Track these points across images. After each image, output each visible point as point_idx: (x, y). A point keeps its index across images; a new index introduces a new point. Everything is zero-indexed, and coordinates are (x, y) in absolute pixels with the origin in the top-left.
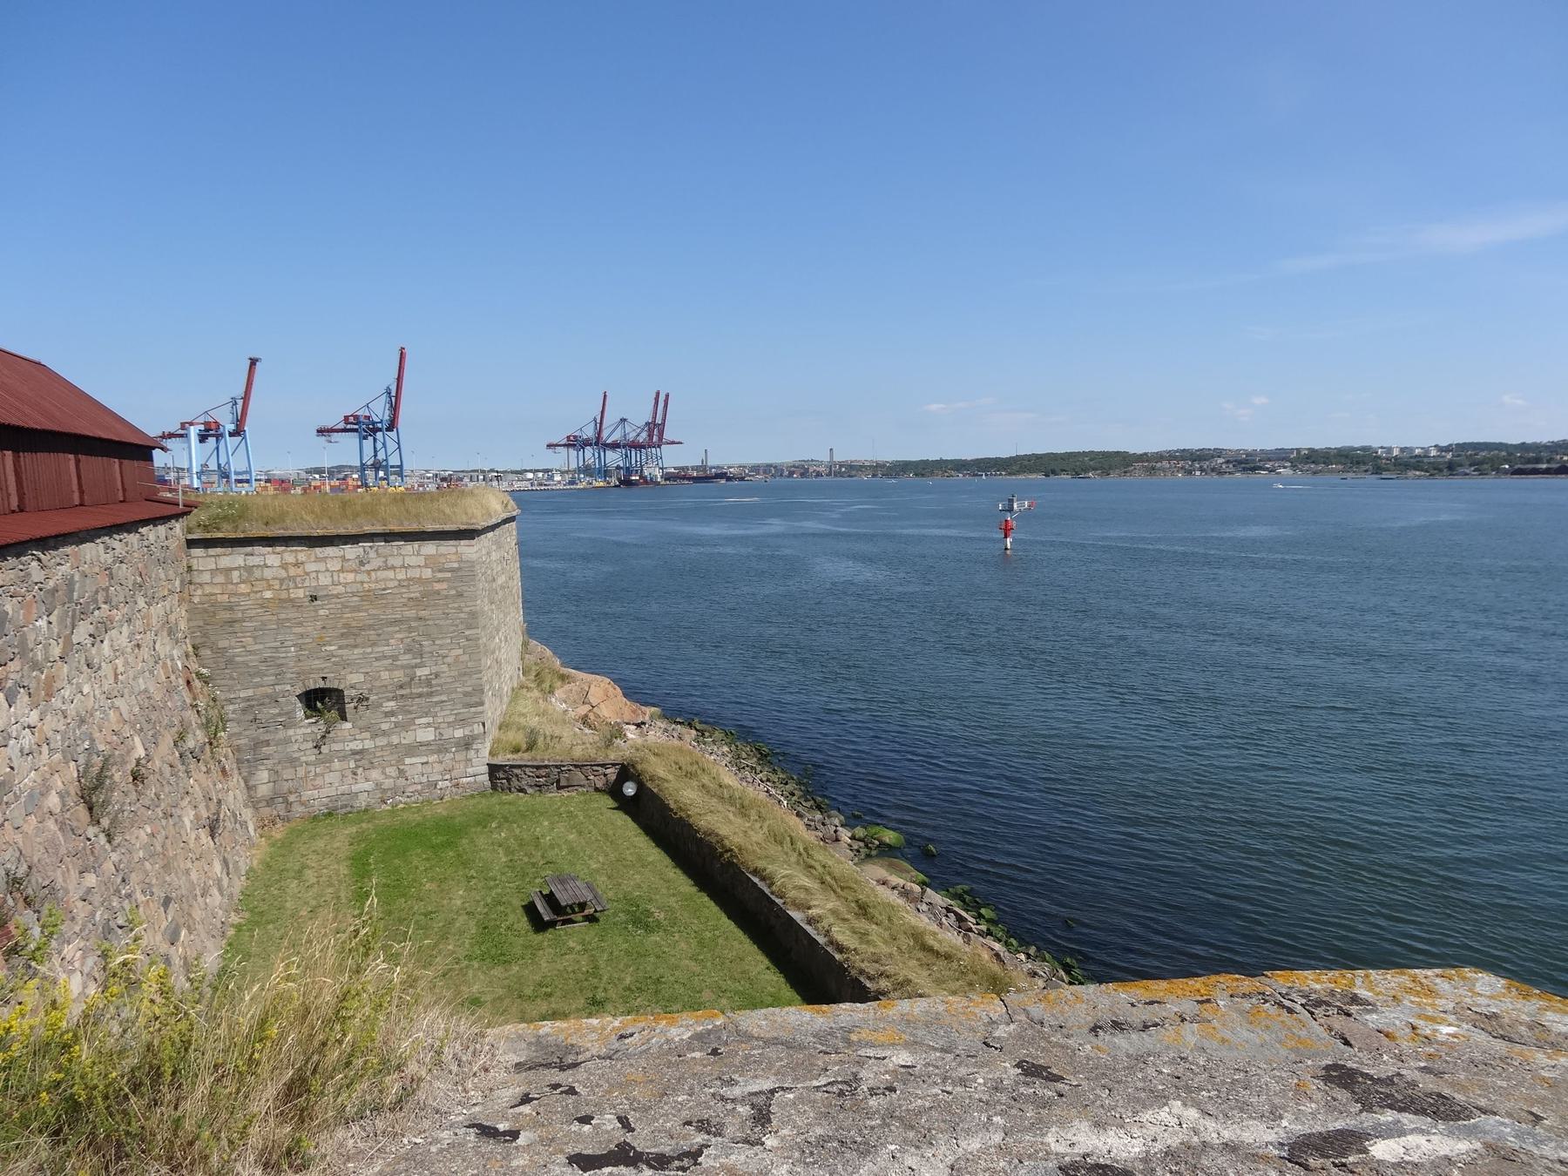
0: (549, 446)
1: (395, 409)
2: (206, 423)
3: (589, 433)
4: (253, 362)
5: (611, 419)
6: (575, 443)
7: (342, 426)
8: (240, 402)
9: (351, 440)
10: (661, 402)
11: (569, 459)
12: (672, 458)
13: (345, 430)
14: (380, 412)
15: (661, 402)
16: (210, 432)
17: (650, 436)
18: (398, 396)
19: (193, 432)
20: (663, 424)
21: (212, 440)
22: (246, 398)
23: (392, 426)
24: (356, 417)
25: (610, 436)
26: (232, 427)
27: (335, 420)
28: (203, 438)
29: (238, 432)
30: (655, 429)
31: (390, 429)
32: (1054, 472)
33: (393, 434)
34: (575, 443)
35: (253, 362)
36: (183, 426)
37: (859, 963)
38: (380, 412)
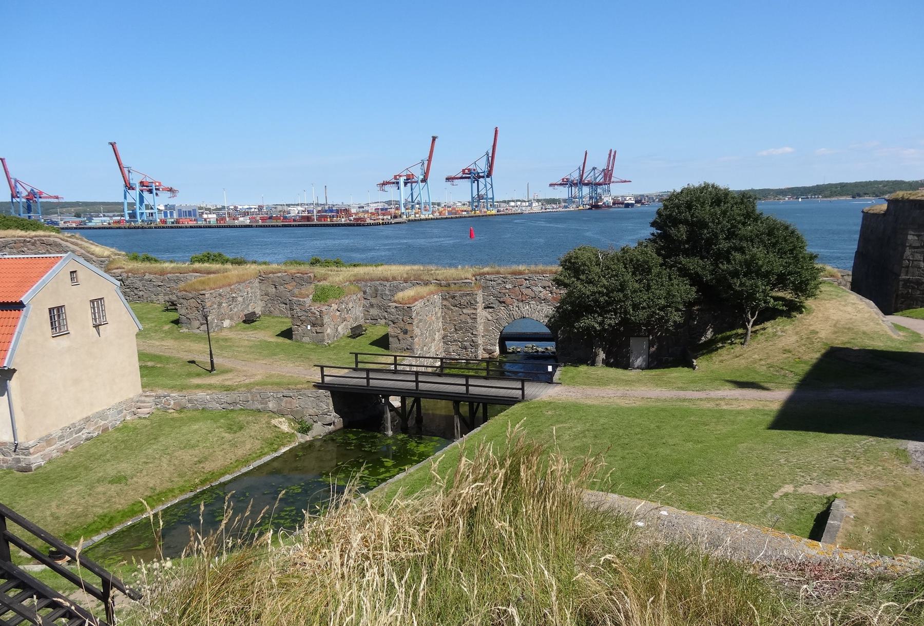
0: (551, 185)
1: (491, 166)
2: (407, 175)
3: (575, 176)
4: (434, 139)
5: (588, 168)
6: (567, 183)
7: (460, 176)
8: (426, 163)
9: (466, 183)
10: (612, 156)
11: (562, 193)
12: (617, 191)
13: (462, 178)
14: (482, 167)
15: (612, 156)
16: (409, 180)
17: (605, 180)
18: (493, 157)
19: (402, 180)
20: (612, 170)
21: (409, 185)
22: (429, 160)
23: (489, 175)
24: (469, 170)
25: (587, 178)
26: (422, 177)
27: (457, 172)
28: (406, 184)
29: (424, 180)
30: (608, 174)
31: (488, 177)
32: (859, 195)
33: (488, 180)
34: (567, 183)
35: (434, 139)
36: (395, 177)
37: (791, 436)
38: (482, 167)
